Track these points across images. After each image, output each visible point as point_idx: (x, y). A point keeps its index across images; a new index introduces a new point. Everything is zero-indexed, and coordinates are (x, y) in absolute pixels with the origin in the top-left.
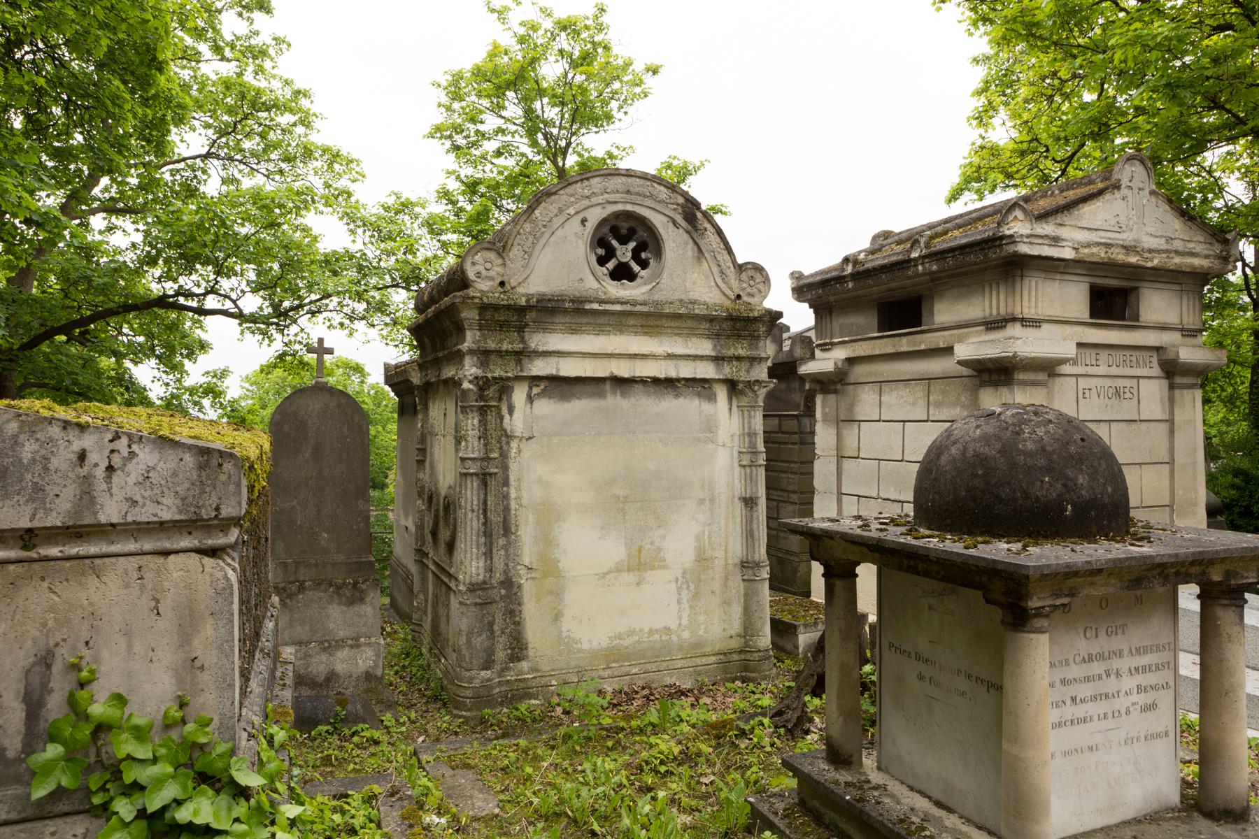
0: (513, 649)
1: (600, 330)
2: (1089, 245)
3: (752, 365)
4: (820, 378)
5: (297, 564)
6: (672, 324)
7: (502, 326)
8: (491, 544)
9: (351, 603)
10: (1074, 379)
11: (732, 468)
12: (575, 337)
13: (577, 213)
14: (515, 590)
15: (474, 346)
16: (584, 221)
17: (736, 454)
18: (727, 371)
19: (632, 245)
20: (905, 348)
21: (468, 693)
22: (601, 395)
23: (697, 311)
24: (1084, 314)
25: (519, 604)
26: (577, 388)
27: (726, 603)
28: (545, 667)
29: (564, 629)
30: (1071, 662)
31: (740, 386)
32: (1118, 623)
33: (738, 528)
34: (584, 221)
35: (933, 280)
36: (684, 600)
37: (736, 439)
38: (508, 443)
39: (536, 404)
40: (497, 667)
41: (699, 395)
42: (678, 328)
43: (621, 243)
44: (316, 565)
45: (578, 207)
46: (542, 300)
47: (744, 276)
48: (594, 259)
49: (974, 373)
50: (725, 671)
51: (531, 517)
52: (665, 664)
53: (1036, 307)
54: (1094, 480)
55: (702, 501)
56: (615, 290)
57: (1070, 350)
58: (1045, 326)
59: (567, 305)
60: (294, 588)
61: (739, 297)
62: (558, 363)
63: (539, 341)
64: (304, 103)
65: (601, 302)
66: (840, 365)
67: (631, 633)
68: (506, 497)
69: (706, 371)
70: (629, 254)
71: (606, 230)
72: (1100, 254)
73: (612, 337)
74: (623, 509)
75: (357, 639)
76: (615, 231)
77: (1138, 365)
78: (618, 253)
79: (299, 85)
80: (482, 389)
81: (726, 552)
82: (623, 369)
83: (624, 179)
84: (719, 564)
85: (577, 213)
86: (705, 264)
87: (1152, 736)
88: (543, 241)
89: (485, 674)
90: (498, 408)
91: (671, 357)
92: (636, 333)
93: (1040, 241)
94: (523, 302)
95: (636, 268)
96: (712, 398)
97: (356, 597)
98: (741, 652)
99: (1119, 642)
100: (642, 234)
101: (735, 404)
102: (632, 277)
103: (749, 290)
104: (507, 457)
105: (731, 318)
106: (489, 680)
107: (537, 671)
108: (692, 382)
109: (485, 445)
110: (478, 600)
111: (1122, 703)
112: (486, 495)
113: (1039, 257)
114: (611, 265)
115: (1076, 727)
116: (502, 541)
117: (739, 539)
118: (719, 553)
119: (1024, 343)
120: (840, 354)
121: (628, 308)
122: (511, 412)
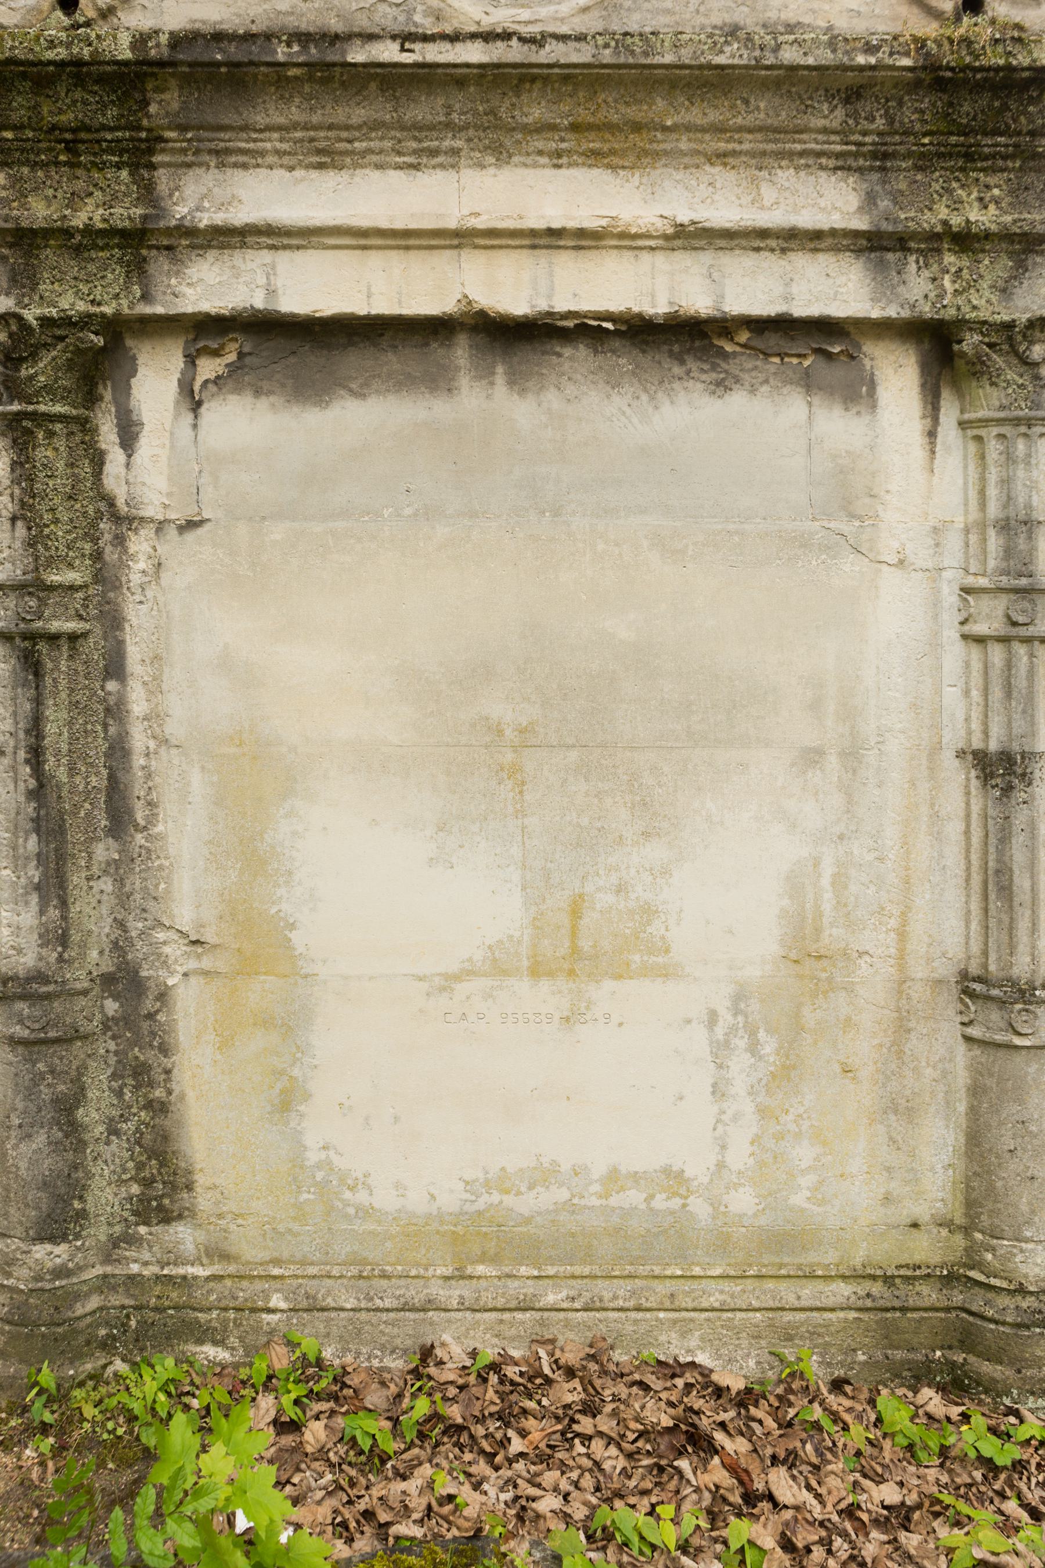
0: (147, 1183)
1: (422, 149)
3: (1021, 267)
6: (695, 115)
11: (935, 644)
12: (330, 179)
14: (149, 1004)
17: (950, 597)
18: (919, 289)
22: (438, 381)
25: (165, 1050)
26: (353, 360)
27: (901, 1109)
28: (251, 1249)
29: (312, 1140)
31: (970, 342)
33: (953, 856)
36: (739, 1086)
37: (954, 542)
38: (120, 541)
39: (211, 412)
40: (99, 1233)
41: (808, 383)
42: (719, 129)
50: (888, 1335)
51: (196, 778)
52: (662, 1288)
55: (812, 757)
59: (281, 53)
62: (271, 271)
63: (199, 195)
67: (544, 1175)
68: (115, 711)
69: (835, 289)
73: (470, 176)
74: (514, 770)
81: (902, 935)
82: (512, 288)
84: (873, 979)
89: (48, 1255)
90: (85, 426)
91: (688, 237)
92: (557, 158)
96: (859, 393)
98: (950, 1279)
101: (950, 413)
104: (116, 585)
106: (60, 1272)
107: (225, 1257)
109: (31, 544)
110: (19, 1031)
112: (38, 701)
116: (104, 851)
117: (953, 895)
118: (877, 940)
121: (513, 53)
122: (128, 437)
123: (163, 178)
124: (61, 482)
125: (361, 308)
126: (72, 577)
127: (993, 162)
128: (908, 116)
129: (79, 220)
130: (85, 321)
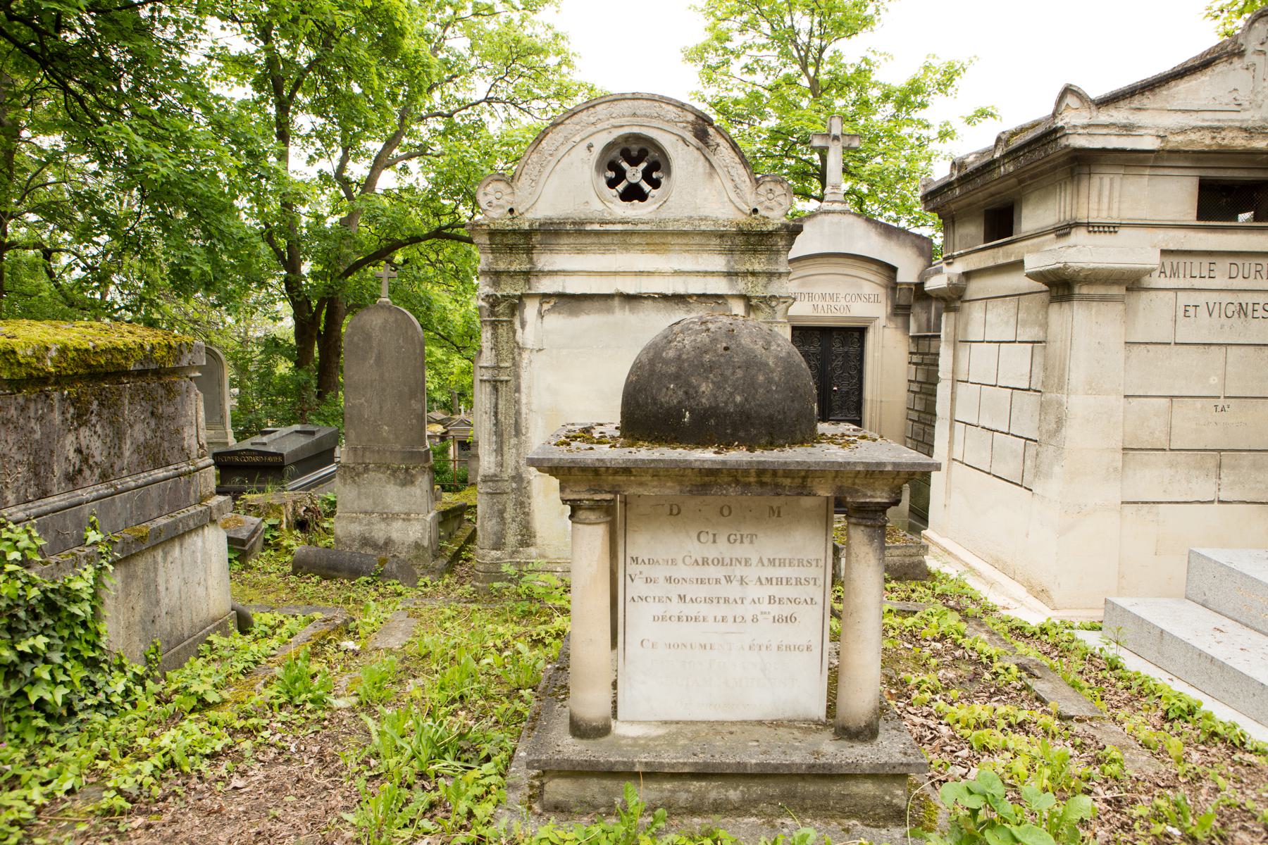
1: (606, 249)
2: (1183, 131)
4: (941, 294)
5: (364, 449)
7: (511, 249)
8: (502, 442)
9: (403, 484)
10: (1172, 294)
13: (583, 140)
14: (525, 485)
15: (486, 268)
16: (590, 147)
18: (741, 286)
19: (643, 165)
20: (1001, 261)
21: (481, 568)
22: (610, 310)
23: (703, 228)
24: (1191, 216)
26: (586, 305)
30: (680, 562)
31: (754, 302)
32: (745, 533)
34: (590, 147)
35: (1020, 182)
38: (520, 354)
43: (631, 165)
44: (378, 451)
45: (583, 135)
46: (545, 224)
47: (762, 189)
48: (603, 181)
49: (1045, 288)
53: (1109, 208)
54: (719, 388)
56: (634, 210)
57: (1152, 259)
58: (1122, 231)
59: (568, 227)
60: (361, 468)
61: (755, 211)
63: (545, 261)
64: (562, 44)
65: (602, 223)
66: (955, 280)
68: (517, 402)
69: (719, 286)
70: (640, 175)
71: (616, 153)
72: (1205, 141)
75: (408, 514)
76: (626, 154)
77: (1174, 274)
78: (628, 175)
79: (558, 29)
80: (493, 306)
82: (630, 286)
83: (630, 103)
85: (583, 140)
86: (717, 180)
87: (788, 648)
88: (549, 169)
90: (511, 322)
91: (677, 273)
93: (1105, 131)
94: (526, 227)
95: (646, 187)
97: (408, 481)
99: (741, 550)
100: (653, 155)
102: (643, 197)
103: (767, 203)
105: (741, 232)
106: (498, 559)
108: (703, 297)
111: (748, 610)
113: (1104, 151)
114: (621, 187)
115: (684, 623)
116: (513, 441)
119: (1080, 251)
120: (959, 267)
122: (523, 325)
123: (535, 257)
124: (505, 339)
125: (588, 292)
126: (507, 365)
127: (761, 252)
128: (737, 241)
129: (512, 269)
130: (514, 296)
